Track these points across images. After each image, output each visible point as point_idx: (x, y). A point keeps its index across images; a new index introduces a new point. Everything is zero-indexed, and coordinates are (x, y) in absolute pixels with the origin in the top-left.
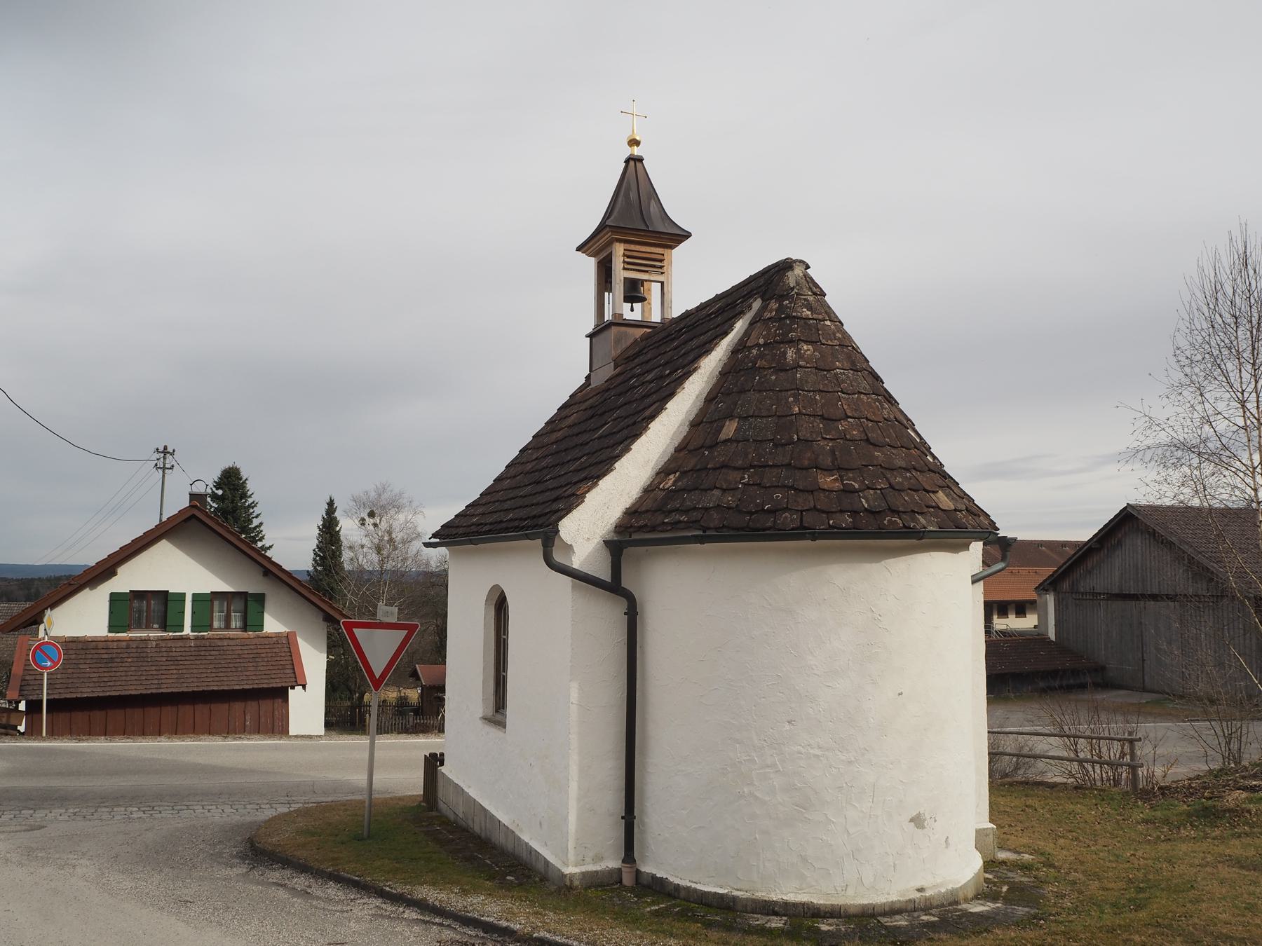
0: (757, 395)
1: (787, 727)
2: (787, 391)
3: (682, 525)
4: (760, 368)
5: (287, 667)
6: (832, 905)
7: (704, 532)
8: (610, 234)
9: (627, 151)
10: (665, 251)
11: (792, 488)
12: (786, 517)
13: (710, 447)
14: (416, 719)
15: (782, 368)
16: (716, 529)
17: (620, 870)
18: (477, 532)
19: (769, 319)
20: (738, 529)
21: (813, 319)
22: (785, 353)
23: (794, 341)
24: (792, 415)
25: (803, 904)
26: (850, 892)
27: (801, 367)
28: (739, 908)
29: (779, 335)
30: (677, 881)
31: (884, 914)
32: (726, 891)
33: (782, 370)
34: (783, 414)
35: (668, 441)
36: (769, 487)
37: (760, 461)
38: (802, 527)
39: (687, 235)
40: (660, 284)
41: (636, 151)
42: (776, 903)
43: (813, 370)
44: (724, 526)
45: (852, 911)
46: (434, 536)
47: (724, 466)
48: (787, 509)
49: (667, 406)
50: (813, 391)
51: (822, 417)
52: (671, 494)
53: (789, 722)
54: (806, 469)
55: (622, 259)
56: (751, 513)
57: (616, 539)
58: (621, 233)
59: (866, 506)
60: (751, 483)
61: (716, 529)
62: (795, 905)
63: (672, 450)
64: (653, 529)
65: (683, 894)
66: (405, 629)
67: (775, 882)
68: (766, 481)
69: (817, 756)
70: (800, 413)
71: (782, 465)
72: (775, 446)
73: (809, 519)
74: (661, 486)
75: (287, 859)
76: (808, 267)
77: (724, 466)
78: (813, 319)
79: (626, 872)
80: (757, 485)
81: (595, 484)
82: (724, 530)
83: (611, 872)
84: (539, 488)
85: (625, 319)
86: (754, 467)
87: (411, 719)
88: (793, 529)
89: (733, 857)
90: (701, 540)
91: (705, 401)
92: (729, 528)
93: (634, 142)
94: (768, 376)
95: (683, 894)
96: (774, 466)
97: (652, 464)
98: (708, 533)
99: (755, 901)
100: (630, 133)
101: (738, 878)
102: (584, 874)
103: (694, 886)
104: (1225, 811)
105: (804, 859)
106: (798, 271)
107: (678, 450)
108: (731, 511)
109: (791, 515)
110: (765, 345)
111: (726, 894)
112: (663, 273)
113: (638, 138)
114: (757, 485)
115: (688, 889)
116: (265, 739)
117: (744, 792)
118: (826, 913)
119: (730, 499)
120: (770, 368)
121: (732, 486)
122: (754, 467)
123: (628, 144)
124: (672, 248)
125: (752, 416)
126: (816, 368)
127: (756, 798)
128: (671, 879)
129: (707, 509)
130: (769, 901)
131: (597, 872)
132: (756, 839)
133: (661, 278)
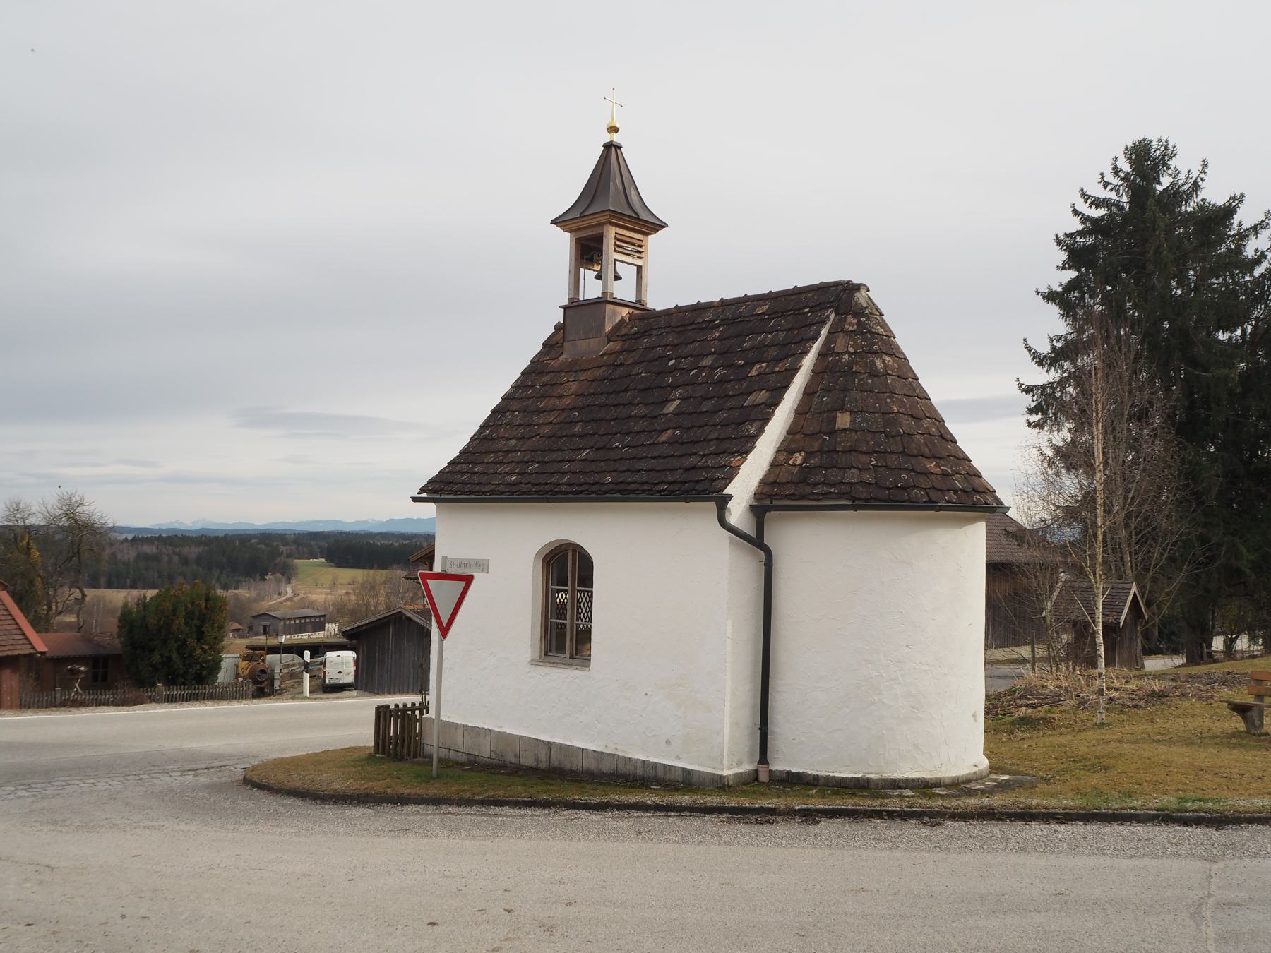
0: (860, 394)
1: (907, 650)
2: (884, 393)
3: (832, 496)
4: (856, 372)
5: (15, 632)
6: (936, 778)
7: (853, 502)
8: (609, 217)
9: (607, 138)
10: (646, 237)
11: (912, 470)
12: (916, 493)
13: (829, 434)
14: (65, 695)
15: (875, 374)
16: (866, 500)
17: (756, 771)
18: (470, 491)
19: (851, 331)
20: (880, 500)
21: (886, 336)
22: (874, 363)
23: (878, 353)
24: (893, 413)
25: (918, 779)
26: (943, 768)
27: (889, 374)
28: (872, 786)
29: (866, 346)
30: (815, 773)
31: (963, 783)
32: (860, 776)
33: (875, 376)
34: (886, 412)
35: (783, 425)
36: (894, 469)
37: (879, 447)
38: (930, 501)
39: (665, 225)
40: (636, 268)
41: (616, 138)
42: (899, 780)
43: (897, 378)
44: (872, 498)
45: (947, 782)
46: (422, 490)
47: (852, 450)
48: (915, 487)
49: (784, 397)
50: (901, 395)
51: (912, 416)
52: (805, 473)
53: (907, 646)
54: (916, 456)
55: (614, 241)
56: (888, 489)
57: (754, 504)
58: (617, 217)
59: (960, 486)
60: (879, 465)
61: (866, 500)
62: (913, 780)
63: (785, 433)
64: (803, 497)
65: (822, 782)
66: (464, 581)
67: (897, 765)
68: (890, 464)
69: (926, 671)
70: (898, 412)
71: (898, 452)
72: (887, 436)
73: (933, 495)
74: (791, 462)
75: (398, 797)
76: (868, 290)
77: (852, 450)
78: (886, 336)
79: (764, 772)
80: (884, 466)
81: (745, 459)
82: (872, 501)
83: (748, 773)
84: (601, 454)
85: (616, 298)
86: (876, 452)
87: (58, 695)
88: (925, 502)
89: (865, 749)
90: (855, 508)
91: (804, 394)
92: (876, 499)
93: (614, 130)
94: (865, 380)
95: (822, 782)
96: (892, 453)
97: (774, 444)
98: (857, 503)
99: (885, 780)
100: (610, 120)
101: (869, 765)
102: (735, 775)
103: (831, 774)
104: (1039, 719)
105: (916, 746)
106: (863, 291)
107: (789, 432)
108: (872, 486)
109: (920, 492)
110: (854, 353)
111: (861, 778)
112: (641, 258)
113: (618, 126)
114: (884, 466)
115: (827, 778)
116: (36, 714)
117: (874, 700)
118: (932, 784)
119: (867, 477)
120: (865, 373)
121: (866, 467)
122: (876, 452)
123: (608, 129)
124: (647, 234)
125: (861, 411)
126: (898, 376)
127: (883, 703)
128: (809, 772)
129: (852, 484)
130: (895, 779)
131: (741, 773)
132: (883, 734)
133: (639, 262)
